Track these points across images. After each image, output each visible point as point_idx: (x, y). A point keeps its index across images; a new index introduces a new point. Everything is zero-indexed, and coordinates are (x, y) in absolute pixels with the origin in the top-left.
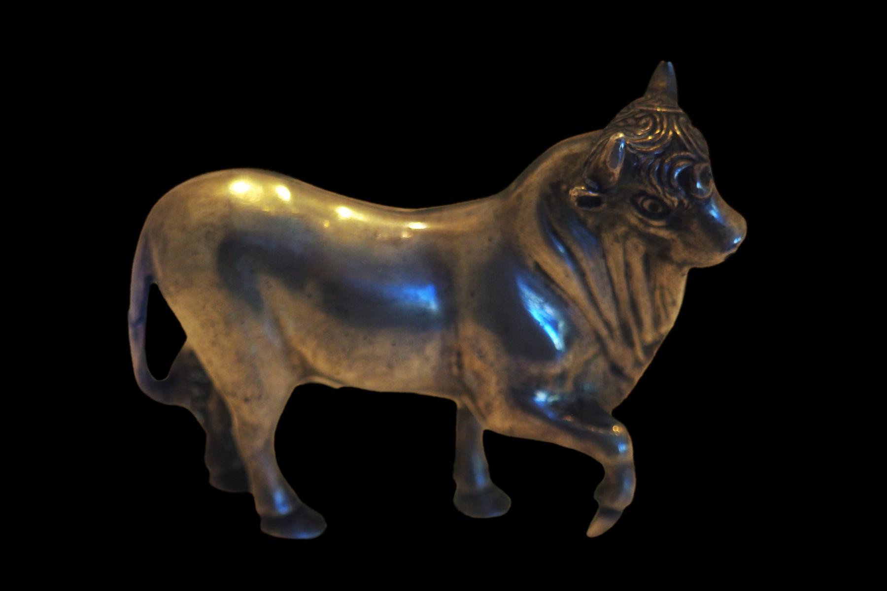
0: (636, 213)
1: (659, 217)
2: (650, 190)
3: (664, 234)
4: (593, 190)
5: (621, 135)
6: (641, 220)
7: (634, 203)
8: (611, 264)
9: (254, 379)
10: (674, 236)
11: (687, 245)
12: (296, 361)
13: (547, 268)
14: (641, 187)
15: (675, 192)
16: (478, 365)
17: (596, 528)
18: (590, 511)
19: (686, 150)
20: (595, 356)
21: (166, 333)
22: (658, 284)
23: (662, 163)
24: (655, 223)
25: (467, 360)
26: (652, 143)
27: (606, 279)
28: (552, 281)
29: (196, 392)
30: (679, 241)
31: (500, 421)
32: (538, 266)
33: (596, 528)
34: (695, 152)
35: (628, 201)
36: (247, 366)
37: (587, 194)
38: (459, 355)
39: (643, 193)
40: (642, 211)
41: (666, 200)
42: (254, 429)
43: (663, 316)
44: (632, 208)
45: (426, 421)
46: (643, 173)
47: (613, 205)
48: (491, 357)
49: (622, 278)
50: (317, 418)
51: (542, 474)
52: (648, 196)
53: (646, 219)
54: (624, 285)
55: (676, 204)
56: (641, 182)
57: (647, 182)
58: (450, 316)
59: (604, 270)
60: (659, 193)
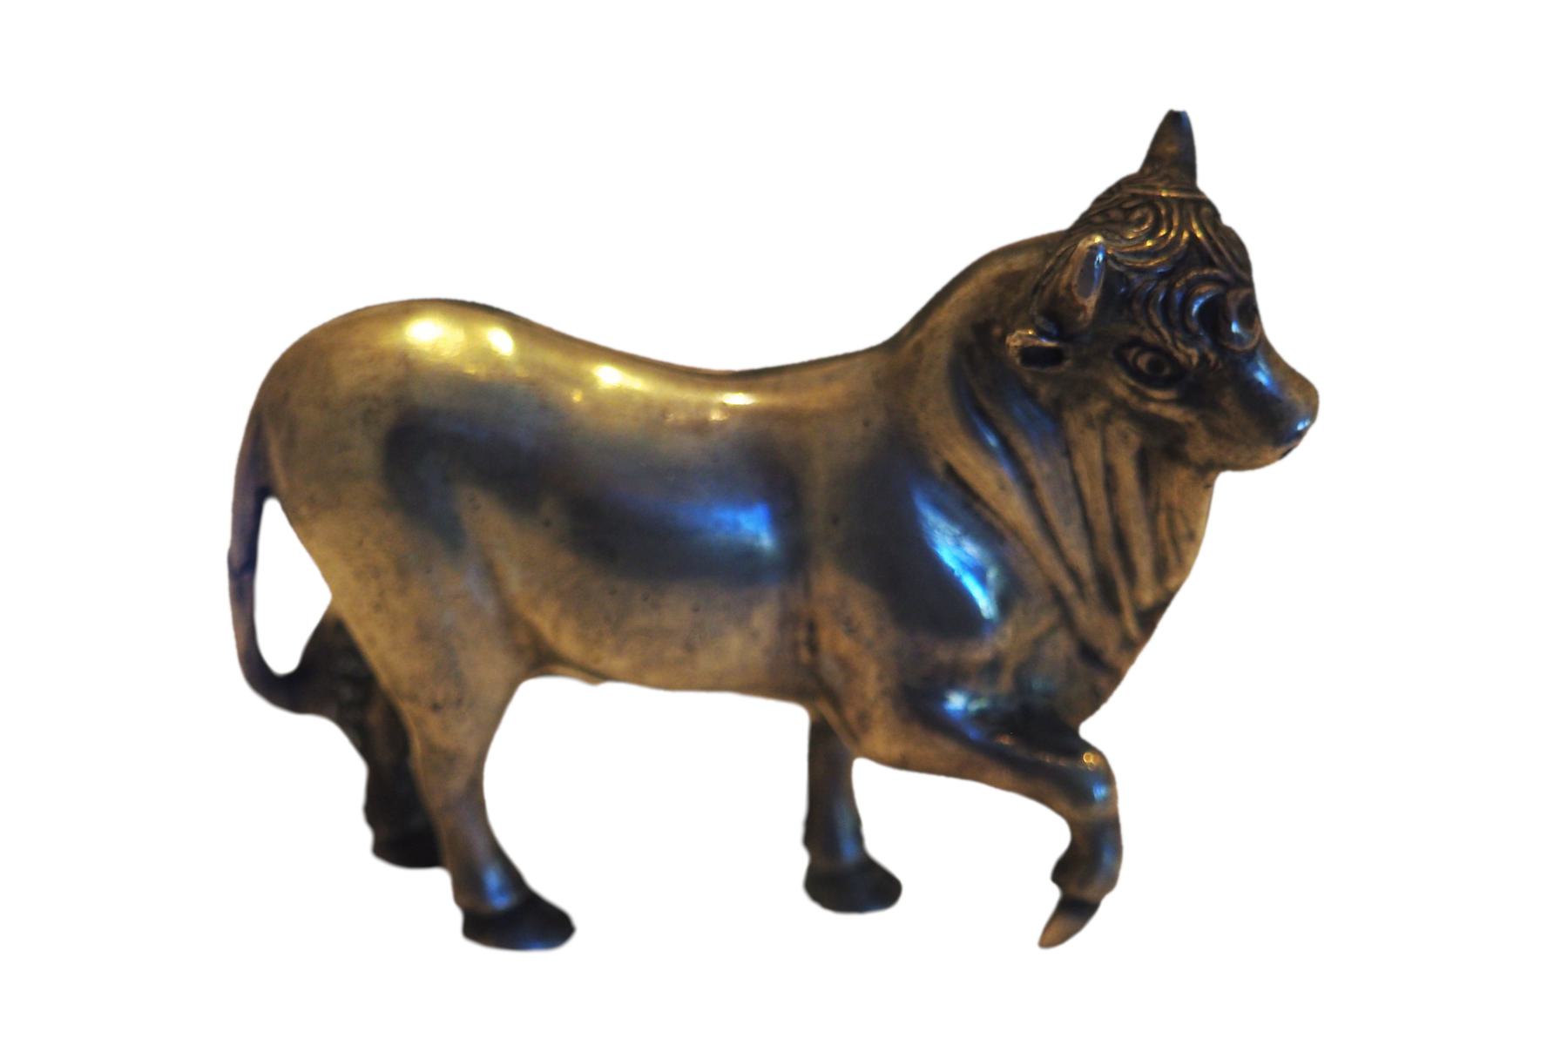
0: (1124, 377)
1: (1165, 384)
2: (1149, 336)
3: (1173, 413)
4: (1049, 337)
5: (1098, 239)
6: (1133, 390)
7: (1121, 359)
8: (1081, 467)
10: (1192, 418)
11: (1215, 433)
13: (967, 474)
14: (1134, 331)
15: (1192, 339)
16: (845, 645)
19: (1212, 265)
20: (1052, 630)
22: (1163, 502)
23: (1170, 288)
24: (1158, 394)
25: (825, 636)
26: (1152, 253)
27: (1071, 493)
28: (977, 497)
30: (1199, 426)
32: (950, 471)
35: (1110, 355)
37: (1037, 342)
38: (812, 627)
39: (1137, 342)
40: (1135, 372)
41: (1177, 354)
44: (1117, 368)
46: (1136, 307)
47: (1083, 362)
48: (868, 632)
49: (1100, 492)
52: (1145, 347)
53: (1141, 387)
54: (1103, 504)
55: (1195, 361)
56: (1134, 322)
57: (1143, 323)
58: (796, 559)
59: (1068, 478)
60: (1165, 341)
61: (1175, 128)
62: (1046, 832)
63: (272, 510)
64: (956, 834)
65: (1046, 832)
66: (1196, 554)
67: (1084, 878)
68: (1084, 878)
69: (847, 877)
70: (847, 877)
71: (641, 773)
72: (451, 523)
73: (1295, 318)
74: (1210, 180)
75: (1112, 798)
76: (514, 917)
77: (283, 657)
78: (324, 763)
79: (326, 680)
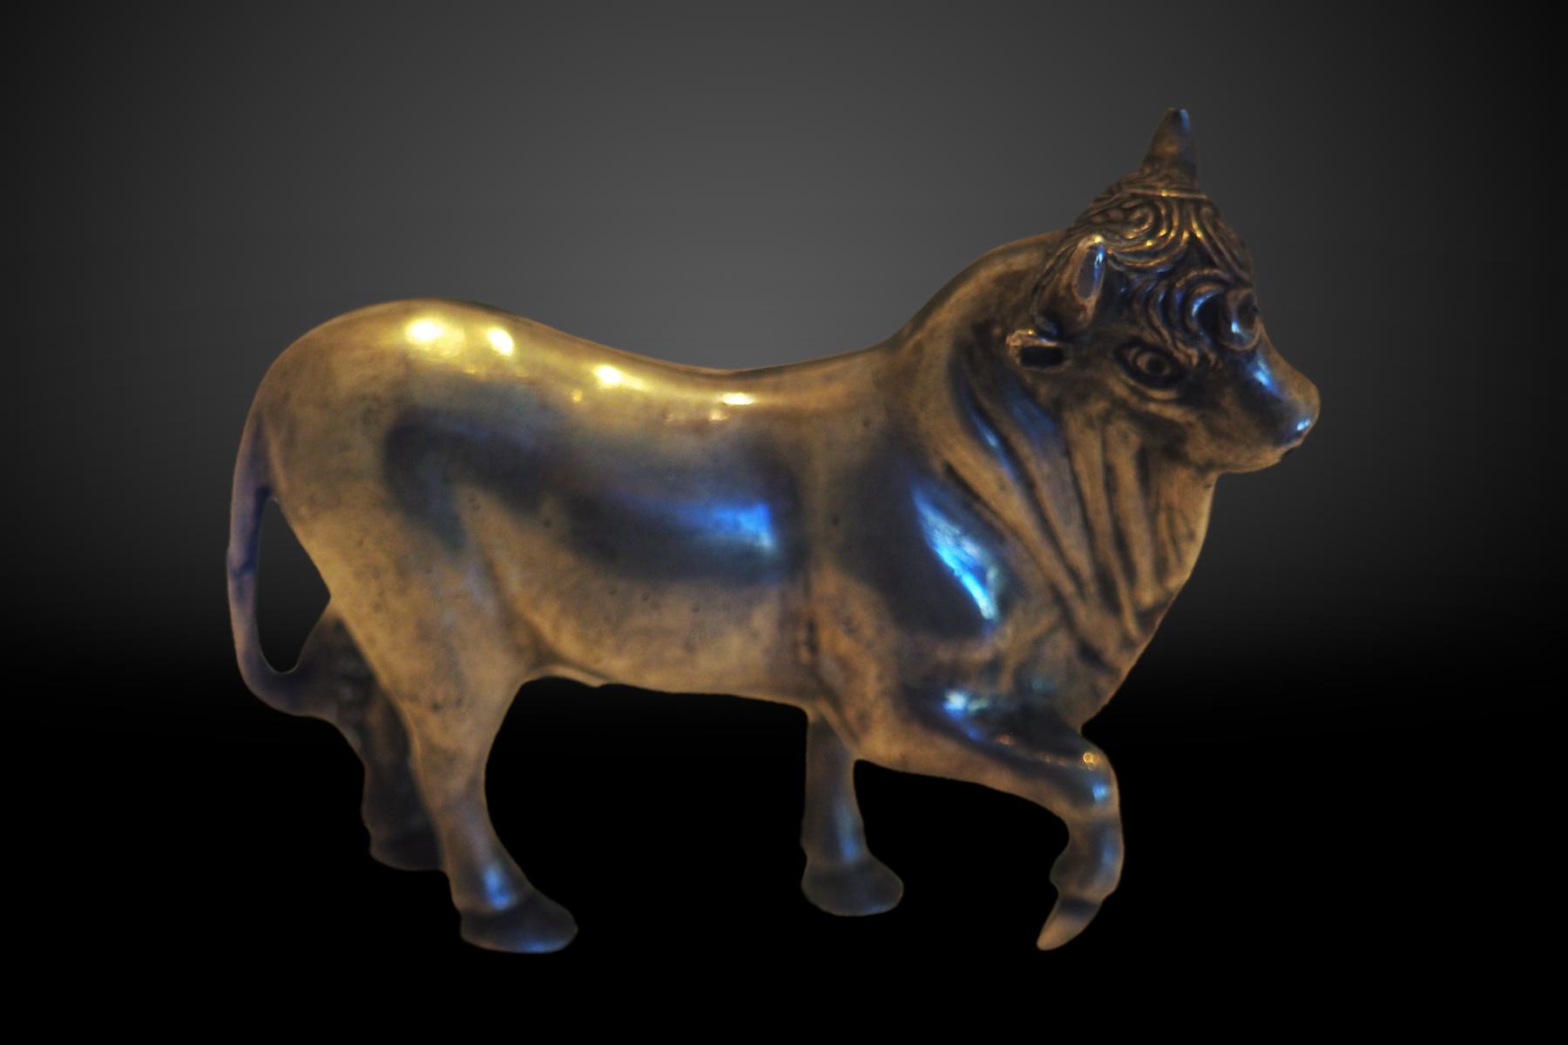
0: (1124, 377)
1: (1165, 384)
2: (1149, 336)
3: (1173, 413)
4: (1049, 337)
5: (1098, 239)
6: (1133, 390)
7: (1121, 359)
8: (1081, 467)
9: (449, 669)
10: (1192, 418)
11: (1215, 433)
12: (523, 639)
13: (967, 474)
14: (1134, 331)
15: (1192, 339)
16: (845, 645)
17: (1054, 934)
18: (1043, 903)
19: (1212, 265)
20: (1052, 630)
21: (294, 595)
22: (1163, 502)
23: (1170, 288)
24: (1158, 394)
25: (825, 636)
26: (1152, 253)
27: (1071, 493)
28: (977, 497)
29: (347, 693)
30: (1199, 426)
31: (885, 745)
32: (950, 471)
33: (1054, 934)
34: (1229, 268)
35: (1110, 355)
36: (439, 650)
37: (1037, 342)
38: (812, 627)
39: (1137, 342)
40: (1135, 372)
41: (1177, 354)
42: (449, 759)
43: (1172, 559)
44: (1117, 368)
45: (750, 750)
46: (1136, 307)
47: (1083, 362)
48: (868, 632)
49: (1100, 492)
50: (561, 744)
51: (958, 839)
52: (1145, 347)
53: (1141, 387)
54: (1103, 504)
55: (1195, 361)
56: (1134, 322)
57: (1143, 323)
58: (796, 559)
59: (1068, 478)
60: (1165, 341)
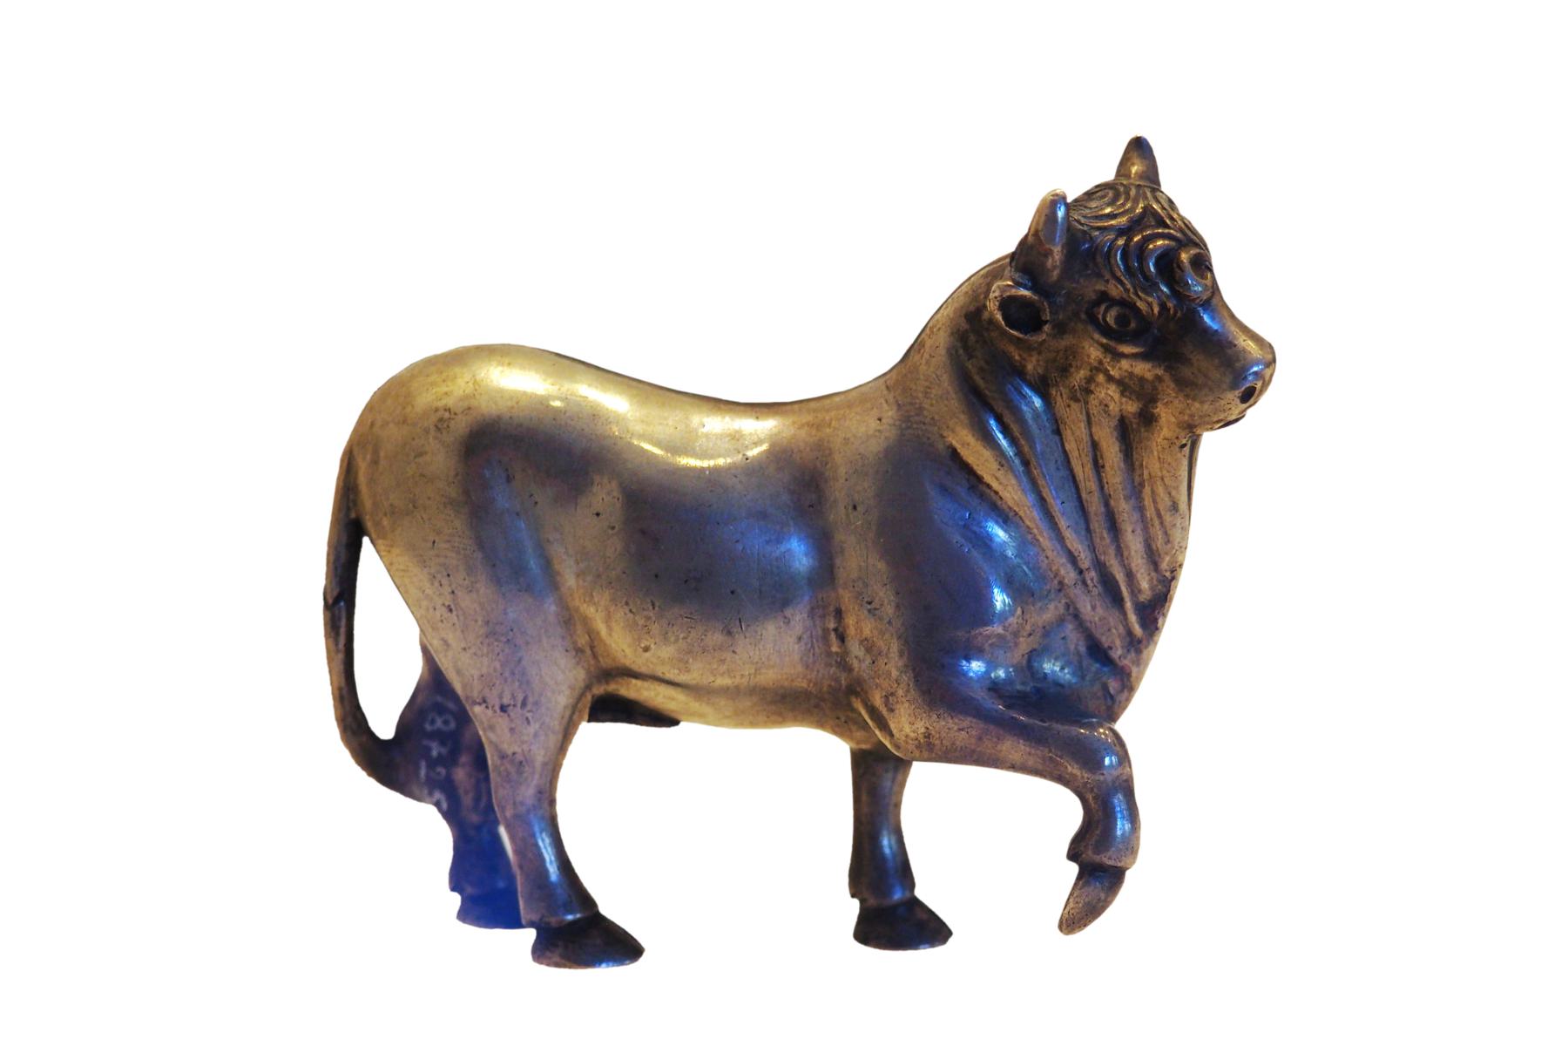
0: (1097, 336)
1: (1133, 338)
2: (1115, 291)
3: (1143, 369)
4: (1025, 287)
6: (1107, 349)
7: (1093, 319)
8: (1070, 446)
10: (1160, 372)
11: (1183, 384)
12: (583, 640)
13: (968, 455)
14: (1100, 287)
15: (1149, 286)
16: (868, 628)
19: (1167, 226)
20: (1061, 621)
22: (1146, 476)
23: (1130, 239)
24: (1127, 349)
25: (850, 621)
26: (1112, 216)
27: (1064, 472)
28: (979, 479)
29: (436, 750)
30: (1167, 377)
32: (954, 454)
35: (1083, 316)
37: (1013, 292)
38: (839, 614)
39: (1104, 297)
40: (1106, 331)
41: (1139, 304)
44: (1090, 328)
46: (1099, 259)
47: (1061, 329)
48: (889, 610)
49: (1089, 467)
52: (1113, 302)
53: (1112, 344)
54: (1092, 485)
55: (1156, 310)
56: (1099, 276)
57: (1107, 276)
58: (825, 573)
59: (1061, 459)
60: (1127, 290)
61: (1139, 147)
62: (1058, 810)
63: (369, 558)
64: (983, 826)
65: (1058, 810)
66: (1185, 530)
67: (1099, 862)
68: (1099, 862)
69: (894, 915)
70: (894, 915)
71: (704, 810)
72: (526, 564)
73: (1247, 288)
74: (1172, 183)
75: (993, 272)
76: (583, 935)
77: (384, 725)
78: (421, 833)
79: (427, 751)
